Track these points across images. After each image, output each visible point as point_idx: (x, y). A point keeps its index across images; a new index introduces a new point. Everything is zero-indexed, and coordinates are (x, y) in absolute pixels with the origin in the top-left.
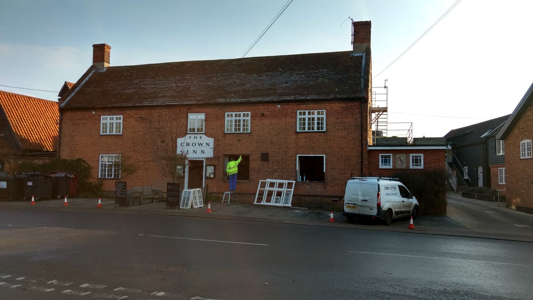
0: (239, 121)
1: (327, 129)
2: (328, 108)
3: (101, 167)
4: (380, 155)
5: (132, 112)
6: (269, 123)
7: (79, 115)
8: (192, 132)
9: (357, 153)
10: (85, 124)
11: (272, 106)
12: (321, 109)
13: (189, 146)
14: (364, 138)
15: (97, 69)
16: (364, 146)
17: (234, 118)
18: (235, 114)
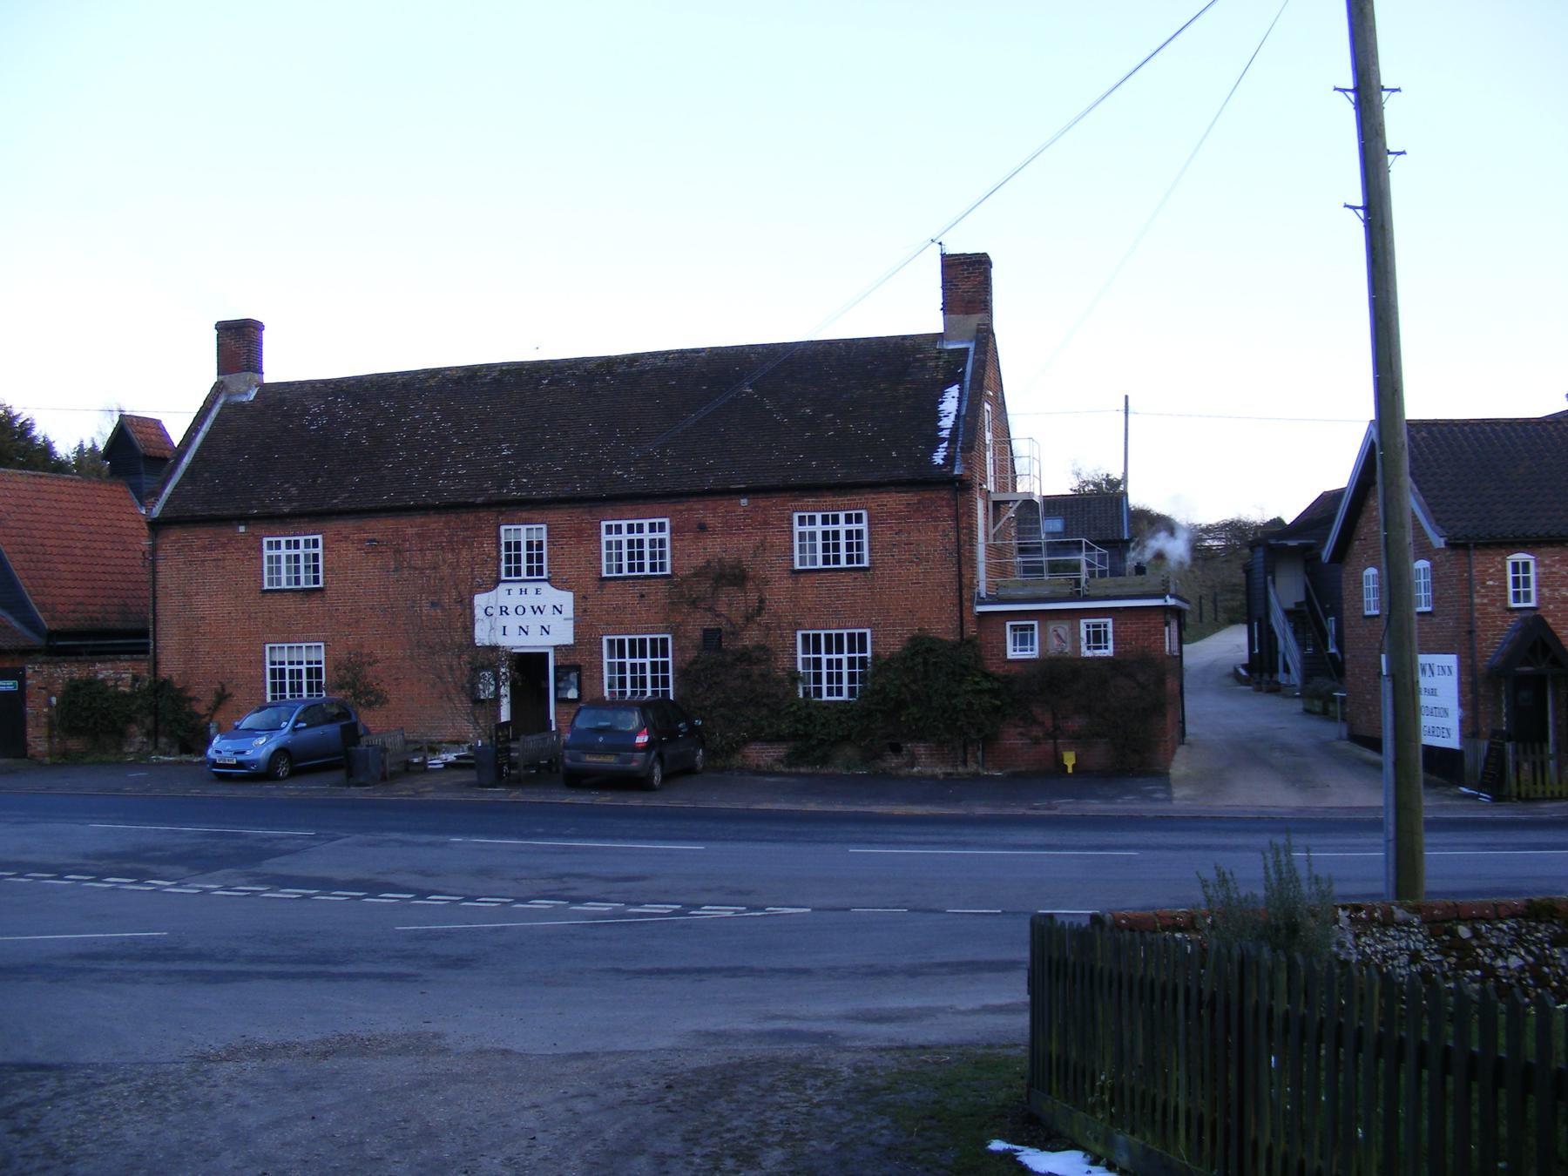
0: (297, 557)
1: (872, 561)
2: (873, 505)
3: (632, 687)
4: (1008, 624)
5: (347, 526)
6: (720, 548)
7: (199, 537)
8: (513, 578)
9: (950, 622)
10: (220, 560)
11: (726, 503)
12: (854, 509)
13: (507, 614)
14: (965, 581)
15: (230, 395)
16: (967, 604)
17: (625, 537)
18: (650, 524)
